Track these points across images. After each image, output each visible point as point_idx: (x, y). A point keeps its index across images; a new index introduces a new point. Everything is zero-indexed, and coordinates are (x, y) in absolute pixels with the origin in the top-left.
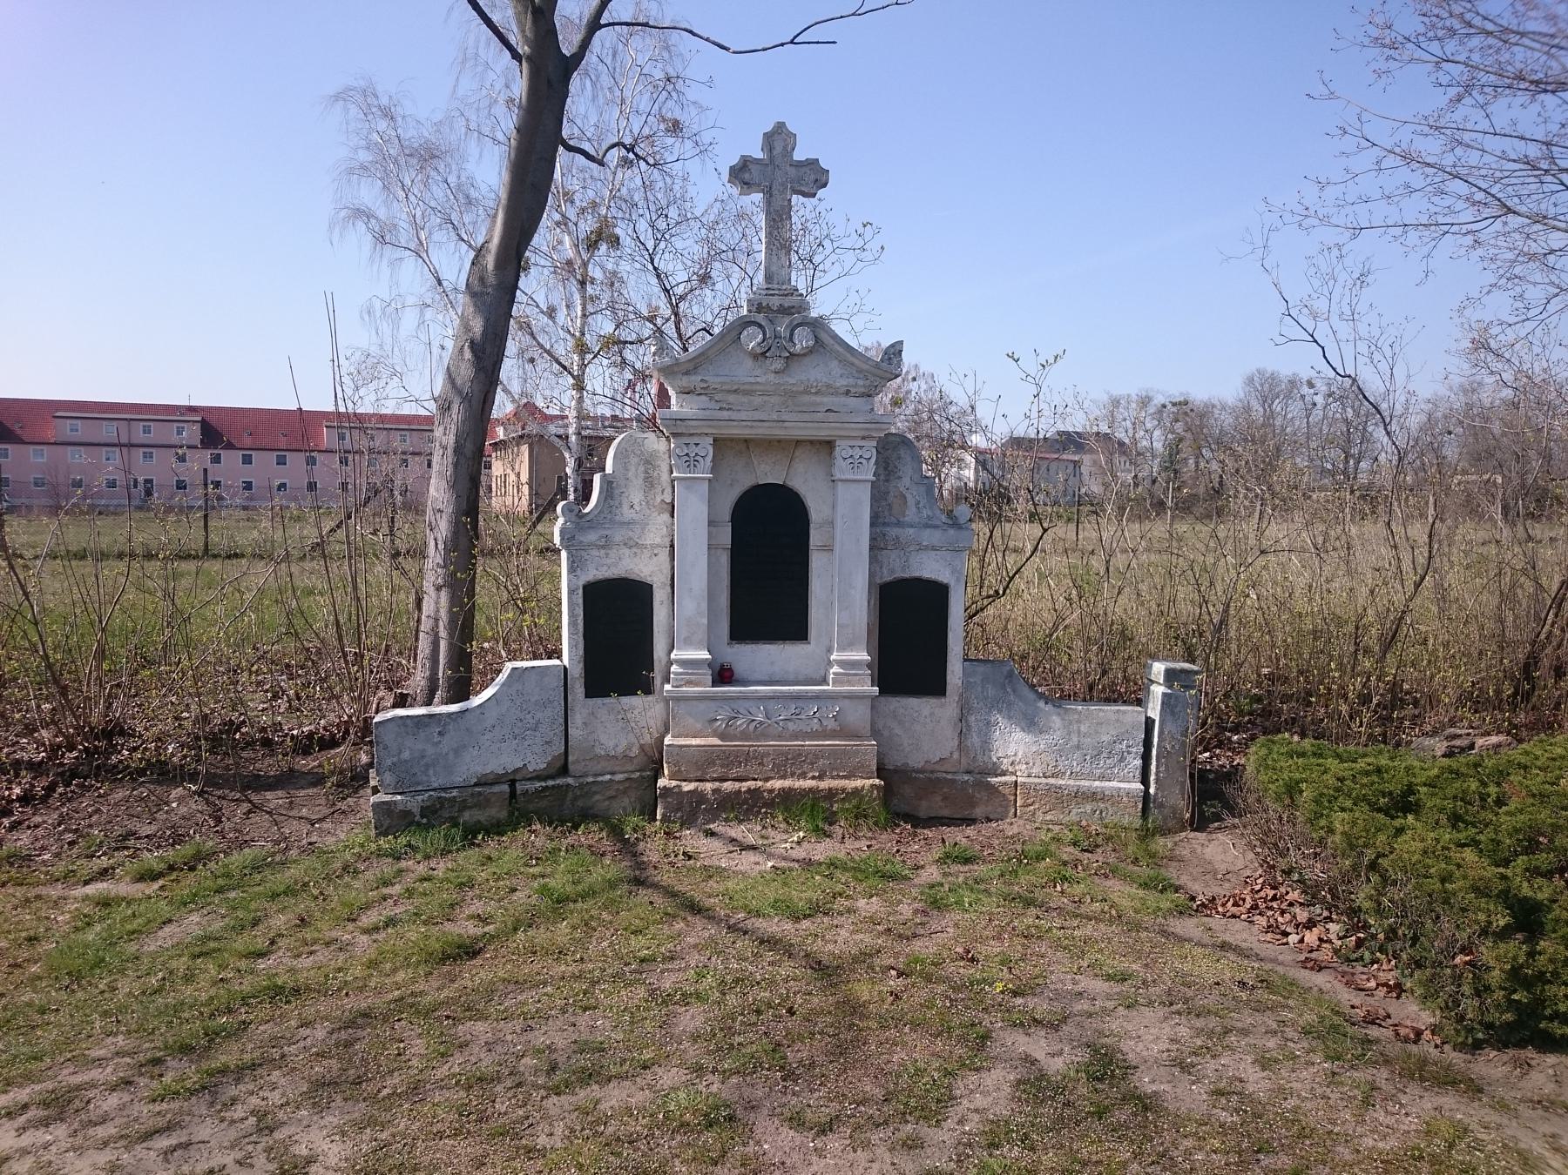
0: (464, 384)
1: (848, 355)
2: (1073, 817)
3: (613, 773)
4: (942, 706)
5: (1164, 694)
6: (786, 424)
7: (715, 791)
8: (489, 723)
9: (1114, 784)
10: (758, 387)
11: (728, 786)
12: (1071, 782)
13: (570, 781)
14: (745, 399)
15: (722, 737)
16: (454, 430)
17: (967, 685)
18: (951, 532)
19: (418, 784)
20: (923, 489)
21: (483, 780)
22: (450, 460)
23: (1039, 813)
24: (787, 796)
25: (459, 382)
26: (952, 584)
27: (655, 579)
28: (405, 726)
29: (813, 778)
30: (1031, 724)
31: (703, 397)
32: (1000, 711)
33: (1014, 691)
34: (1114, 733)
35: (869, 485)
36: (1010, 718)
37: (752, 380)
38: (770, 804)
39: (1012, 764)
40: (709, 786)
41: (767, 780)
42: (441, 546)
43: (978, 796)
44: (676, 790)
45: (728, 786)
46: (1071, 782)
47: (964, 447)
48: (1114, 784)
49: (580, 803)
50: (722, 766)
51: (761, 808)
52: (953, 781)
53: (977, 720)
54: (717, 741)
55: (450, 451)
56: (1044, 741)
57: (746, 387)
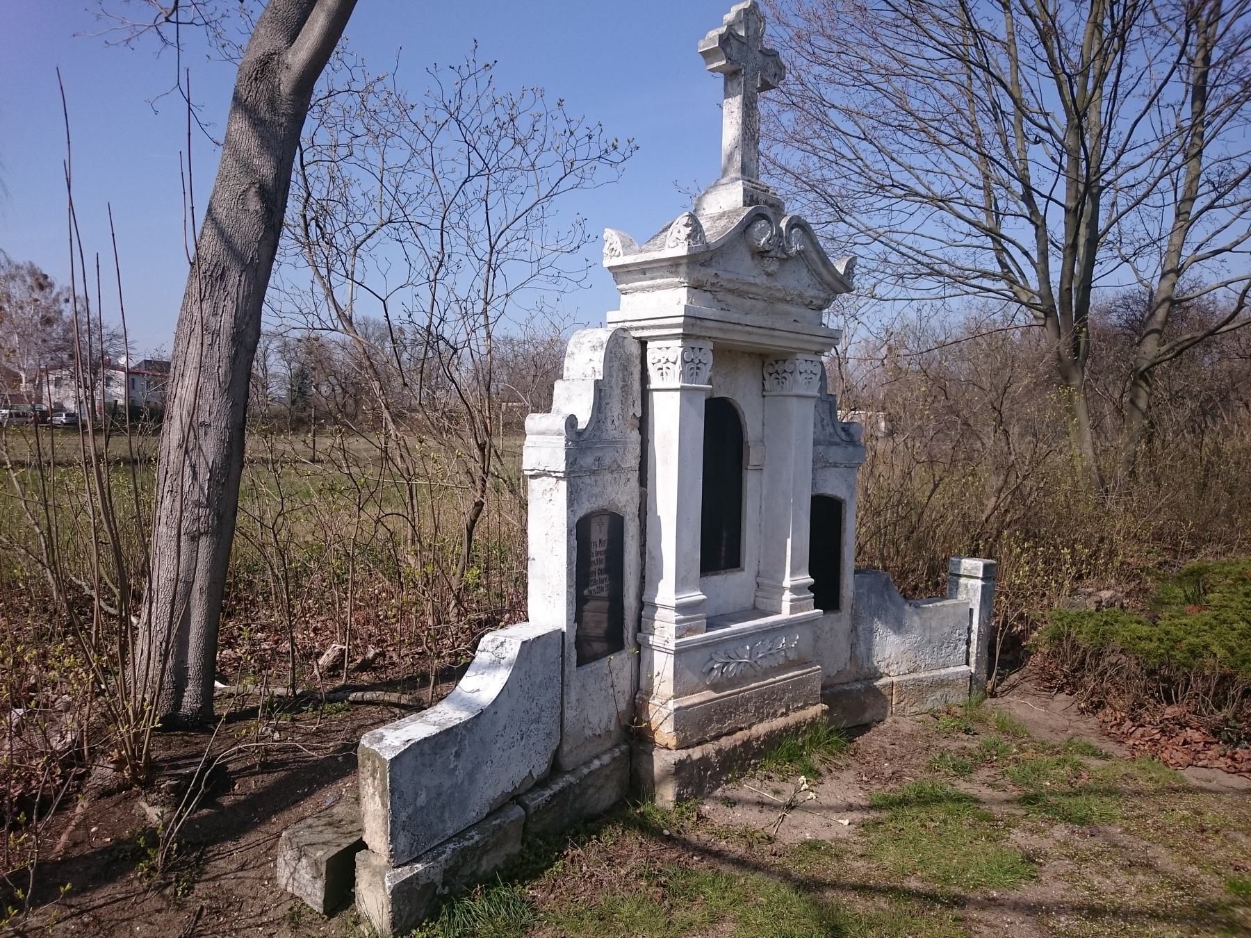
0: (246, 244)
1: (820, 264)
2: (929, 705)
3: (597, 757)
4: (839, 620)
5: (983, 587)
6: (776, 333)
7: (719, 752)
8: (500, 727)
9: (951, 670)
10: (754, 289)
11: (725, 742)
12: (927, 674)
13: (570, 778)
14: (739, 301)
15: (715, 687)
16: (230, 307)
17: (857, 597)
18: (850, 449)
19: (435, 836)
20: (827, 406)
21: (494, 807)
22: (225, 352)
23: (908, 707)
24: (773, 741)
25: (239, 242)
26: (847, 500)
27: (628, 509)
28: (422, 754)
29: (782, 715)
30: (898, 626)
31: (708, 294)
32: (879, 619)
33: (890, 597)
34: (951, 624)
35: (812, 403)
36: (887, 623)
37: (751, 280)
38: (759, 754)
39: (888, 666)
40: (710, 748)
41: (750, 727)
42: (204, 476)
43: (867, 701)
44: (689, 761)
45: (725, 742)
46: (927, 674)
47: (117, 367)
48: (951, 670)
49: (577, 806)
50: (718, 722)
51: (751, 760)
52: (851, 691)
53: (864, 629)
54: (711, 694)
55: (224, 338)
56: (913, 638)
57: (745, 288)
